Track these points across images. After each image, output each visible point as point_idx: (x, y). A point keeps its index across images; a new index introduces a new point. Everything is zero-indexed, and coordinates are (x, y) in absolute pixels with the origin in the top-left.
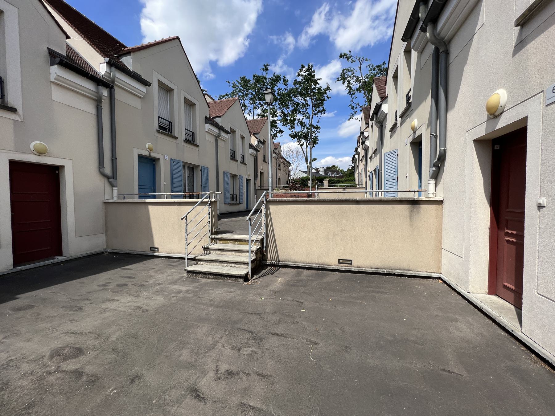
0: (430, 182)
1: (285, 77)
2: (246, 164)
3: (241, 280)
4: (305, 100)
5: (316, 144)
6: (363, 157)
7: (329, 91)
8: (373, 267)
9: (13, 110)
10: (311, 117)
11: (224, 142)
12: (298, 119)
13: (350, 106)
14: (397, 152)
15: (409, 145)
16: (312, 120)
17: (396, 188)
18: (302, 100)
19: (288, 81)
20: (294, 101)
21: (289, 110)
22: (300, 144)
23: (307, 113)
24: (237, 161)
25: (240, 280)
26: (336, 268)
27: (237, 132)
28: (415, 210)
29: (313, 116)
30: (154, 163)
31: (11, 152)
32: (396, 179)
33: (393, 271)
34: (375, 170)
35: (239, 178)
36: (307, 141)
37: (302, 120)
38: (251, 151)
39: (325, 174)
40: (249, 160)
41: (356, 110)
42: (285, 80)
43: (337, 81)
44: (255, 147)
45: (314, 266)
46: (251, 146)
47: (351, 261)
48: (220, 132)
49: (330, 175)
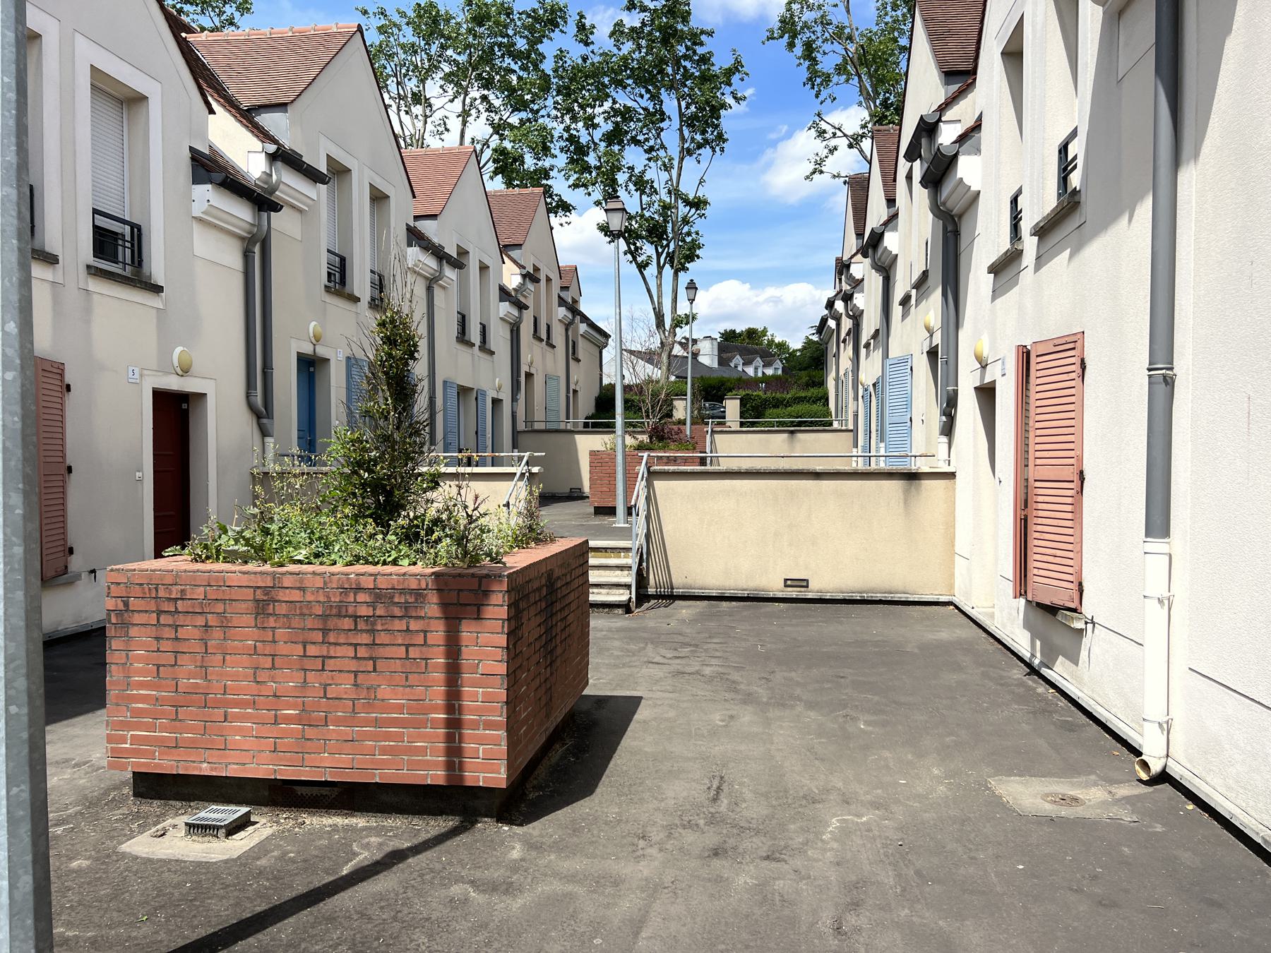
0: (940, 440)
1: (582, 17)
2: (492, 353)
3: (620, 611)
4: (655, 97)
5: (693, 260)
6: (848, 334)
7: (742, 80)
8: (845, 590)
9: (157, 289)
10: (676, 163)
11: (297, 215)
12: (629, 168)
13: (813, 130)
14: (909, 360)
15: (925, 354)
16: (679, 175)
17: (908, 449)
18: (642, 96)
19: (595, 31)
20: (614, 102)
21: (598, 134)
22: (636, 263)
23: (663, 147)
24: (357, 300)
25: (616, 612)
26: (780, 595)
27: (355, 175)
28: (913, 488)
29: (682, 159)
30: (312, 369)
31: (154, 373)
32: (909, 422)
33: (879, 596)
34: (874, 385)
35: (476, 399)
36: (660, 250)
37: (644, 172)
38: (505, 308)
39: (720, 363)
40: (500, 339)
41: (833, 143)
42: (584, 25)
43: (768, 39)
44: (513, 294)
45: (740, 594)
46: (504, 293)
47: (807, 581)
48: (441, 266)
49: (740, 368)
